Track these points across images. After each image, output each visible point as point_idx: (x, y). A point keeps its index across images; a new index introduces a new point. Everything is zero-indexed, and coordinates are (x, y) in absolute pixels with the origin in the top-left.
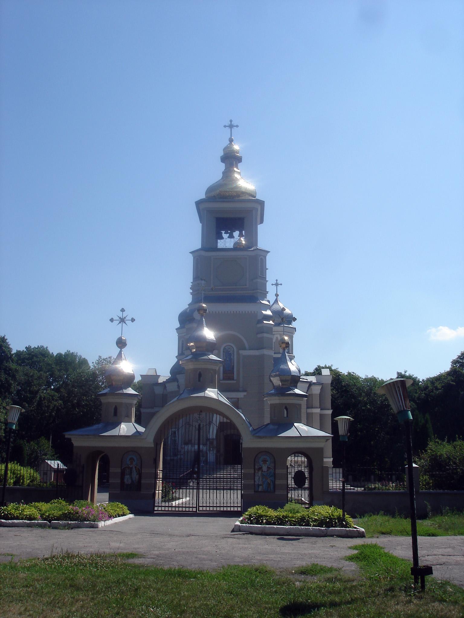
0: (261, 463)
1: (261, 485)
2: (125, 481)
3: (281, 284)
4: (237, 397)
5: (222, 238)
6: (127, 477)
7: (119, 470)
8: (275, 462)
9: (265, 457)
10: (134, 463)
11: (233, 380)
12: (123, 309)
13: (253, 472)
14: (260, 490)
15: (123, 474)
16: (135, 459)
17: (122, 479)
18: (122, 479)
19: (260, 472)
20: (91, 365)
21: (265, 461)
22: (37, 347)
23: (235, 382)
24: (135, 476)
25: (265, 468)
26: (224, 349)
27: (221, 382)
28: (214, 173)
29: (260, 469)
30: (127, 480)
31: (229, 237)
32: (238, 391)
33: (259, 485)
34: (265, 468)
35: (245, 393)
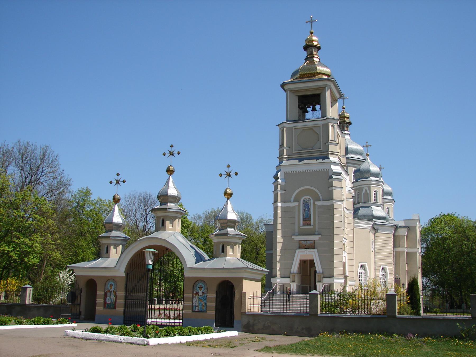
0: (198, 289)
1: (197, 306)
2: (107, 301)
3: (370, 146)
4: (314, 239)
5: (308, 112)
6: (108, 298)
7: (103, 293)
8: (207, 289)
9: (201, 284)
10: (113, 288)
11: (311, 225)
12: (238, 174)
13: (191, 296)
14: (196, 310)
15: (105, 296)
16: (114, 285)
17: (105, 299)
18: (105, 299)
19: (197, 296)
20: (189, 217)
21: (201, 287)
22: (446, 214)
23: (312, 227)
24: (113, 297)
25: (200, 293)
26: (304, 201)
27: (301, 227)
28: (298, 61)
29: (197, 293)
30: (108, 301)
31: (312, 110)
32: (314, 234)
33: (196, 306)
34: (200, 293)
35: (320, 236)
